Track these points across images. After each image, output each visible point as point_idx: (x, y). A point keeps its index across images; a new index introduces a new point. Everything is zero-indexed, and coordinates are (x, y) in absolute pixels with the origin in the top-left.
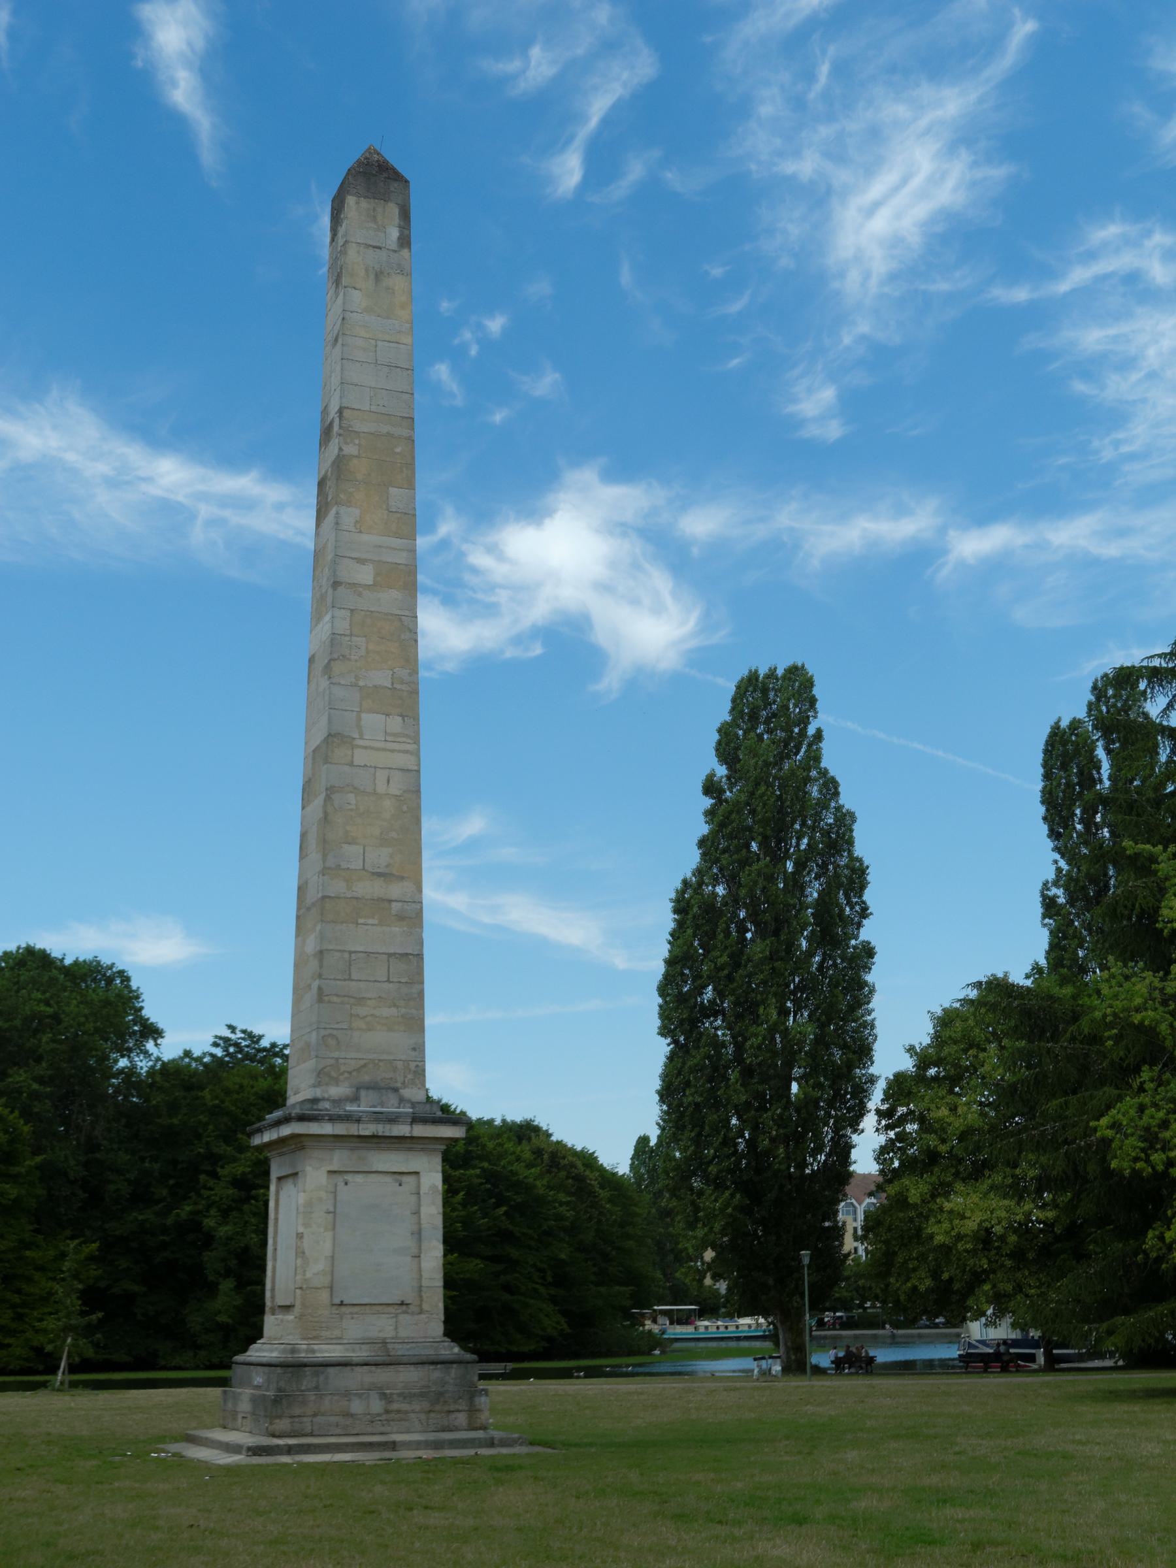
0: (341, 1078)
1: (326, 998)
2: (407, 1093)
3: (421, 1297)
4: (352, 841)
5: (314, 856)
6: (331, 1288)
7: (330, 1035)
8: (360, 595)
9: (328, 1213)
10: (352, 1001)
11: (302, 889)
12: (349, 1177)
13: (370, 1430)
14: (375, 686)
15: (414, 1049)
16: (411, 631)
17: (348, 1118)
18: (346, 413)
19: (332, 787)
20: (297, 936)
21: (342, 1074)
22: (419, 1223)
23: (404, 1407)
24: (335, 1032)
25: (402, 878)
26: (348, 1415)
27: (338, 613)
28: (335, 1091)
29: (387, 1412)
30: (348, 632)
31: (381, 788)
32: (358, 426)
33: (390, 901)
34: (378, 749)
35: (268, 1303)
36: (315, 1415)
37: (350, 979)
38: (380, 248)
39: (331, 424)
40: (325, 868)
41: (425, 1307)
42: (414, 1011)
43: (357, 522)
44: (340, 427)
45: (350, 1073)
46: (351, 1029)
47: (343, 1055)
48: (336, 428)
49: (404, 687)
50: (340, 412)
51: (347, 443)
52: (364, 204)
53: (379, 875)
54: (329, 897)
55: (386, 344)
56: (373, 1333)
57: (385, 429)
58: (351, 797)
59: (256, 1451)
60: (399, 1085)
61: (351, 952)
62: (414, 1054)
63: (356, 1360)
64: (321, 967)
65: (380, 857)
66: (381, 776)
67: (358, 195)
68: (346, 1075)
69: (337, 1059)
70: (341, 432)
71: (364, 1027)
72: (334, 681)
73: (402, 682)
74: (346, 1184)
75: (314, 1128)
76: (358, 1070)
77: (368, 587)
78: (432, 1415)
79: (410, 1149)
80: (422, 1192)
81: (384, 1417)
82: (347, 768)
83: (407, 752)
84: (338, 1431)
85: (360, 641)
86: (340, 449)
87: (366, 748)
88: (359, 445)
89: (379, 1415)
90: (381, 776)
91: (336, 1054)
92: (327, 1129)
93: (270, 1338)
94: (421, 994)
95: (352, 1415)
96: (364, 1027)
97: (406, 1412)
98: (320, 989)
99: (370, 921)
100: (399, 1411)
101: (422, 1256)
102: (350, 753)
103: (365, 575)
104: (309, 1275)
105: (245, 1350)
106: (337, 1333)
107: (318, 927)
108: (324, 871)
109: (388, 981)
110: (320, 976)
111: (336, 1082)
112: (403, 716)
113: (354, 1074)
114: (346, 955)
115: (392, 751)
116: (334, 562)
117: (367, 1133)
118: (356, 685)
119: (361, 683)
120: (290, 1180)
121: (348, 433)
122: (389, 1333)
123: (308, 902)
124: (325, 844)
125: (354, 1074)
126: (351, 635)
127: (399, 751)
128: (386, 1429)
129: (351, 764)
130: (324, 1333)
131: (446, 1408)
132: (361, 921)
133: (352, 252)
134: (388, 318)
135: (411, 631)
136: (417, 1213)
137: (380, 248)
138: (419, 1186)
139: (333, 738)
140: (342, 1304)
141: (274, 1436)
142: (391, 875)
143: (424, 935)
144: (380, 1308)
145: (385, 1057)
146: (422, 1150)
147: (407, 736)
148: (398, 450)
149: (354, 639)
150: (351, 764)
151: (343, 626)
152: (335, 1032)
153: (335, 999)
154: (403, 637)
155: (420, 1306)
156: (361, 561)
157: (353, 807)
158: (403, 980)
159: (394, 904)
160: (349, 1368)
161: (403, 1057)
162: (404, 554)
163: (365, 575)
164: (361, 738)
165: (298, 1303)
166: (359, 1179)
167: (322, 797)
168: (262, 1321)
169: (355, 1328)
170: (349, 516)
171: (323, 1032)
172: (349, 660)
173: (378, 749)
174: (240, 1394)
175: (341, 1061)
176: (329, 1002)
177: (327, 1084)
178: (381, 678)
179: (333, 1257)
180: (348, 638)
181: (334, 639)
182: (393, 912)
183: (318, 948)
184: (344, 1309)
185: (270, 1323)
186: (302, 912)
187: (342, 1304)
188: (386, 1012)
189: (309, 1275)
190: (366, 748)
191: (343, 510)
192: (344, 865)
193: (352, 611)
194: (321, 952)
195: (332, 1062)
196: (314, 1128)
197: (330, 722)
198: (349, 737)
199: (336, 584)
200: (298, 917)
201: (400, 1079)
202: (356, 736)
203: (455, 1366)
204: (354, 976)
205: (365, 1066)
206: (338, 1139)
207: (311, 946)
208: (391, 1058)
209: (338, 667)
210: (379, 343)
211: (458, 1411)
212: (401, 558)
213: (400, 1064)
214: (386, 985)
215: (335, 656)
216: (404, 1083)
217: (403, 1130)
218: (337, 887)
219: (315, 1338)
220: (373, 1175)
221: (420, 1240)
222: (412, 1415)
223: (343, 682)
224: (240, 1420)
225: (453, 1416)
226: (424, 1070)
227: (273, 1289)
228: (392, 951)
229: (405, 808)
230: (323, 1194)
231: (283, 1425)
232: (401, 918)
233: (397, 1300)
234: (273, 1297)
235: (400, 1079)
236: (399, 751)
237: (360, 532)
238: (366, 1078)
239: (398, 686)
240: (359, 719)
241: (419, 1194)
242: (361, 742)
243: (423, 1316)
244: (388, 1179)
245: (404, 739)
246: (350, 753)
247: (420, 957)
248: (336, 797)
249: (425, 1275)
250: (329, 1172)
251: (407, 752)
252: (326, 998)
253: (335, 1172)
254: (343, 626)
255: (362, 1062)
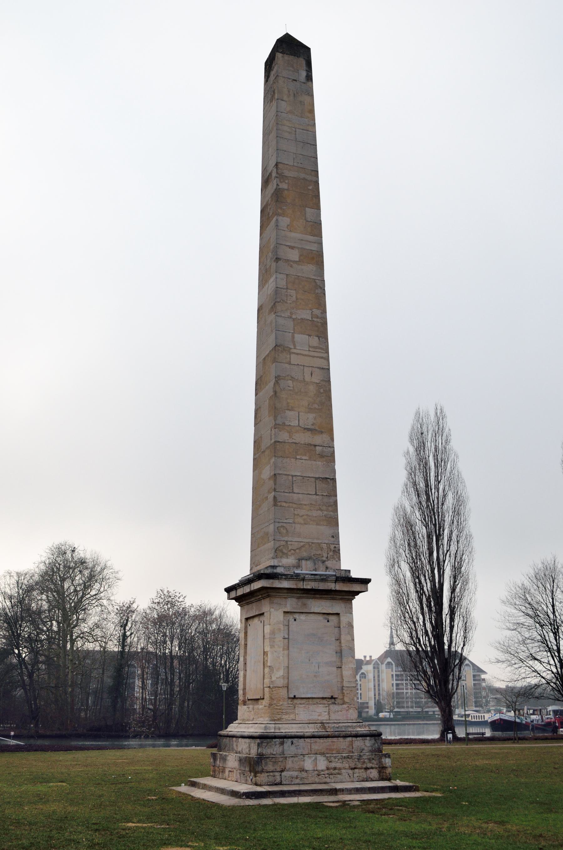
0: (289, 553)
1: (279, 504)
2: (329, 563)
3: (343, 693)
4: (292, 409)
5: (268, 420)
6: (288, 687)
7: (282, 526)
8: (291, 266)
9: (285, 638)
10: (295, 506)
11: (257, 444)
12: (296, 616)
13: (317, 780)
14: (302, 319)
15: (333, 537)
16: (321, 288)
17: (297, 577)
18: (280, 166)
19: (279, 376)
20: (254, 470)
21: (290, 551)
22: (341, 646)
23: (338, 765)
24: (285, 525)
25: (322, 432)
26: (302, 770)
27: (280, 276)
28: (290, 561)
29: (328, 769)
30: (285, 287)
31: (308, 378)
32: (287, 173)
33: (315, 446)
34: (306, 355)
35: (241, 697)
36: (282, 771)
37: (293, 492)
38: (296, 81)
39: (270, 174)
40: (276, 424)
41: (346, 699)
42: (332, 513)
43: (288, 225)
44: (277, 173)
45: (295, 550)
46: (294, 523)
47: (290, 539)
48: (274, 174)
49: (318, 320)
50: (277, 165)
51: (281, 182)
52: (286, 57)
53: (309, 430)
54: (279, 442)
55: (301, 130)
56: (315, 717)
57: (302, 175)
58: (290, 382)
59: (249, 795)
60: (324, 559)
61: (293, 476)
62: (332, 539)
63: (307, 734)
64: (275, 484)
65: (309, 419)
66: (307, 371)
67: (283, 53)
68: (292, 551)
69: (287, 542)
70: (278, 176)
71: (303, 522)
72: (278, 314)
73: (317, 317)
74: (295, 620)
75: (277, 584)
76: (300, 548)
77: (295, 262)
78: (356, 770)
79: (333, 599)
80: (341, 627)
81: (327, 772)
82: (287, 365)
83: (322, 358)
84: (298, 781)
85: (293, 293)
86: (277, 185)
87: (298, 354)
88: (288, 183)
89: (322, 771)
90: (307, 371)
91: (286, 539)
92: (285, 584)
93: (243, 720)
94: (336, 503)
95: (306, 771)
96: (303, 522)
97: (340, 769)
98: (275, 497)
99: (304, 458)
100: (335, 769)
101: (343, 667)
102: (288, 356)
103: (294, 255)
104: (274, 679)
105: (226, 728)
106: (292, 716)
107: (273, 460)
108: (276, 426)
109: (316, 494)
110: (275, 490)
111: (286, 555)
112: (319, 337)
113: (297, 551)
114: (290, 478)
115: (314, 357)
116: (276, 247)
117: (309, 587)
118: (291, 317)
119: (294, 317)
120: (256, 620)
121: (281, 177)
122: (324, 717)
123: (263, 447)
124: (275, 411)
125: (297, 551)
126: (287, 288)
127: (317, 357)
128: (328, 780)
129: (290, 363)
130: (284, 717)
131: (364, 766)
132: (298, 457)
133: (281, 80)
134: (301, 117)
135: (321, 288)
136: (338, 639)
137: (296, 81)
138: (339, 622)
139: (278, 348)
140: (295, 697)
141: (256, 784)
142: (316, 430)
143: (336, 467)
144: (318, 701)
145: (315, 541)
146: (341, 599)
147: (323, 349)
148: (310, 188)
149: (289, 291)
150: (290, 363)
151: (282, 283)
152: (285, 525)
153: (284, 504)
154: (317, 291)
155: (343, 699)
156: (292, 248)
157: (292, 389)
158: (325, 494)
159: (317, 448)
160: (302, 739)
161: (327, 542)
162: (316, 245)
163: (294, 255)
164: (295, 348)
165: (267, 696)
166: (303, 617)
167: (271, 384)
168: (237, 709)
169: (304, 713)
170: (284, 221)
171: (277, 525)
172: (287, 303)
173: (306, 355)
174: (226, 755)
175: (289, 543)
176: (281, 506)
177: (281, 557)
178: (305, 314)
179: (288, 667)
180: (285, 291)
181: (277, 291)
182: (317, 453)
183: (272, 473)
184: (295, 701)
185: (242, 711)
186: (257, 455)
187: (295, 697)
188: (315, 513)
189: (274, 679)
190: (298, 354)
191: (280, 218)
192: (287, 423)
193: (287, 275)
194: (275, 474)
195: (284, 543)
196: (277, 584)
197: (276, 338)
198: (288, 347)
199: (277, 259)
200: (254, 459)
201: (325, 555)
202: (292, 347)
203: (368, 738)
204: (296, 490)
205: (303, 546)
206: (290, 590)
207: (267, 473)
208: (320, 542)
209: (279, 307)
210: (297, 130)
211: (372, 768)
212: (314, 247)
213: (325, 546)
214: (314, 497)
215: (278, 300)
216: (327, 558)
217: (332, 586)
218: (284, 436)
219: (279, 720)
220: (311, 615)
221: (341, 657)
222: (343, 771)
223: (283, 315)
224: (227, 773)
225: (369, 771)
226: (339, 550)
227: (244, 689)
228: (317, 476)
229: (322, 391)
230: (281, 626)
231: (263, 777)
232: (321, 456)
233: (328, 695)
234: (244, 694)
235: (325, 555)
236: (317, 357)
237: (290, 231)
238: (305, 554)
239: (315, 320)
240: (293, 337)
241: (339, 627)
242: (295, 351)
243: (345, 706)
244: (321, 618)
245: (320, 350)
246: (288, 356)
247: (334, 480)
248: (282, 382)
249: (345, 679)
250: (284, 612)
251: (322, 358)
252: (279, 504)
253: (288, 612)
254: (282, 283)
255: (302, 544)
